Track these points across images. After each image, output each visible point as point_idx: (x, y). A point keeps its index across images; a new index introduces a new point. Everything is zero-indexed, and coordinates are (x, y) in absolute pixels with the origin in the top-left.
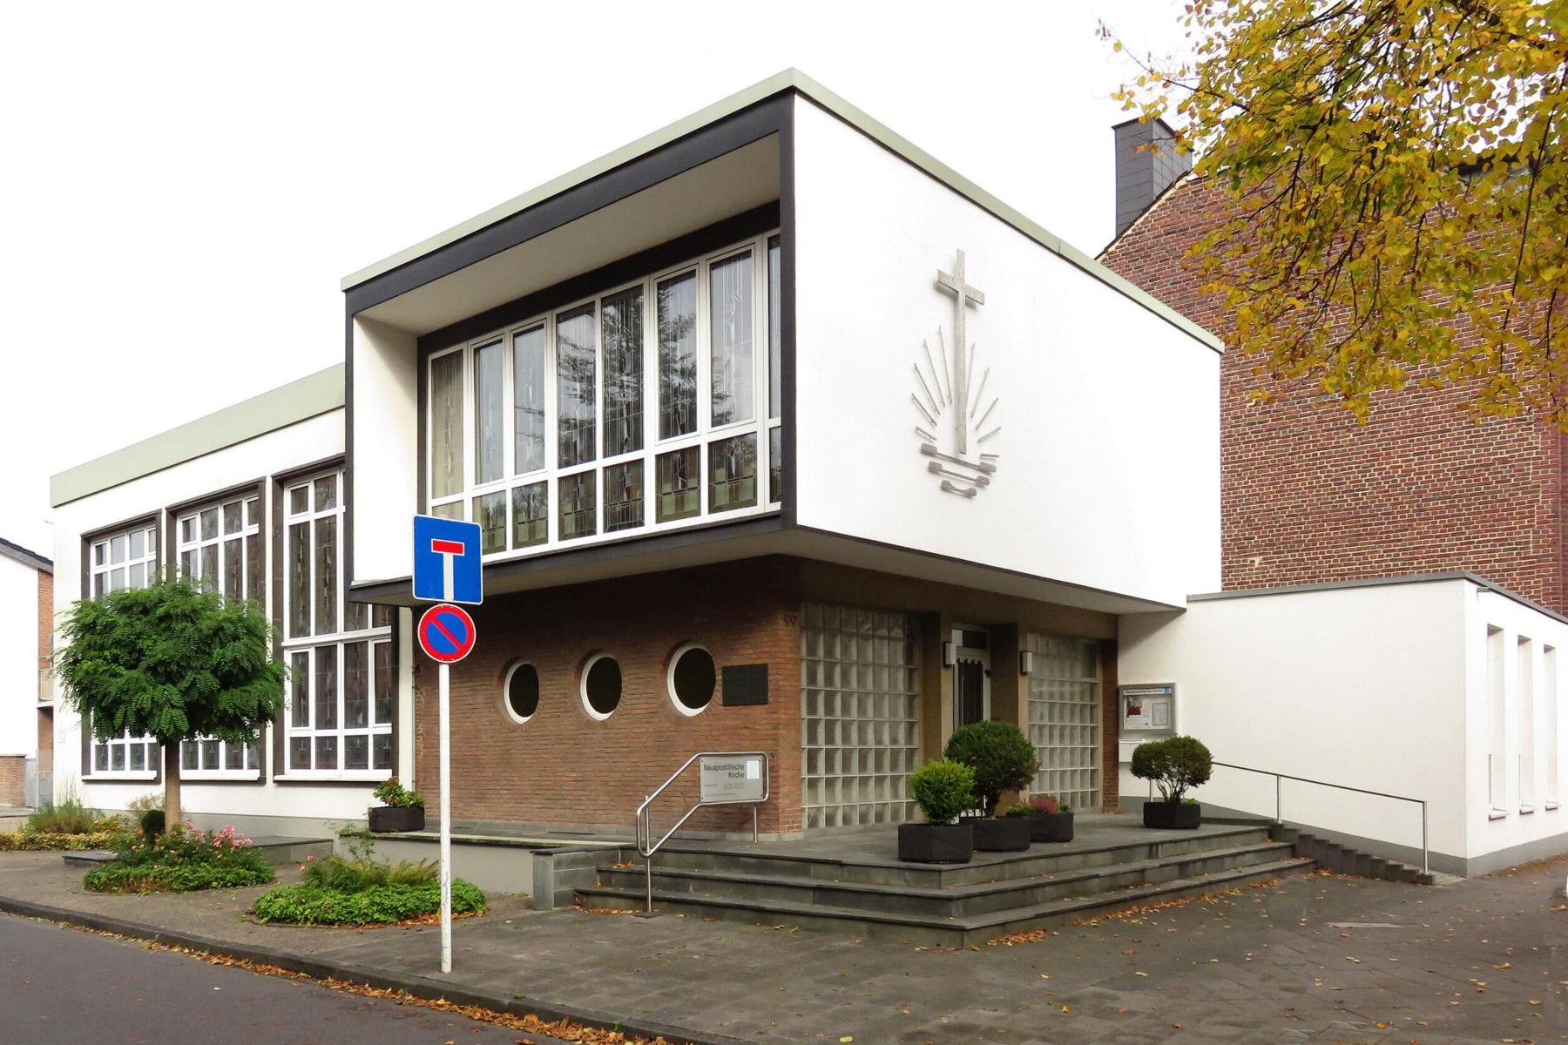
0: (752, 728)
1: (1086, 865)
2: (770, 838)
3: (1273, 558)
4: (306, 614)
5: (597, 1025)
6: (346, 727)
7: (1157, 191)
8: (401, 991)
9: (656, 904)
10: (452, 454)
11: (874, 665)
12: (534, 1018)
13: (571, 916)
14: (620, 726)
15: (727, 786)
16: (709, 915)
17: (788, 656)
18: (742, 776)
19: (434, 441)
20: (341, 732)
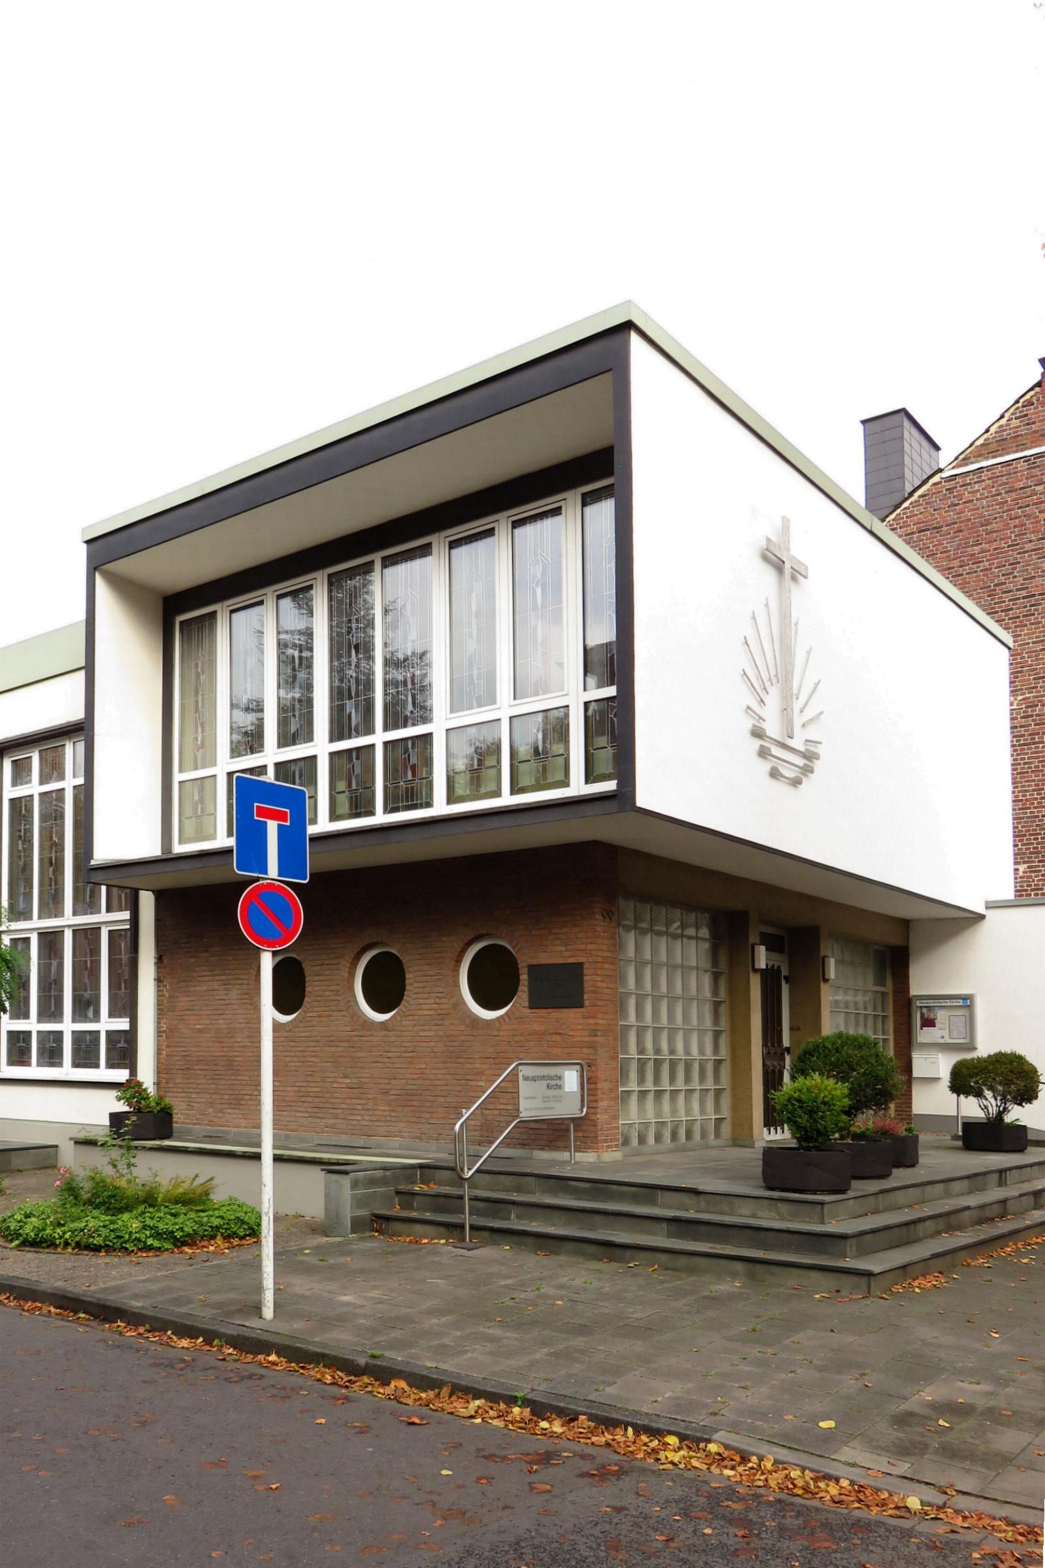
0: (564, 1034)
1: (948, 1194)
2: (588, 1157)
3: (1039, 866)
4: (28, 896)
5: (493, 1397)
6: (74, 1021)
7: (909, 489)
8: (216, 1342)
9: (475, 1233)
10: (202, 725)
11: (682, 966)
12: (403, 1384)
13: (369, 1244)
14: (404, 1029)
15: (546, 1099)
16: (541, 1248)
17: (605, 954)
18: (560, 1087)
19: (182, 706)
20: (68, 1026)
